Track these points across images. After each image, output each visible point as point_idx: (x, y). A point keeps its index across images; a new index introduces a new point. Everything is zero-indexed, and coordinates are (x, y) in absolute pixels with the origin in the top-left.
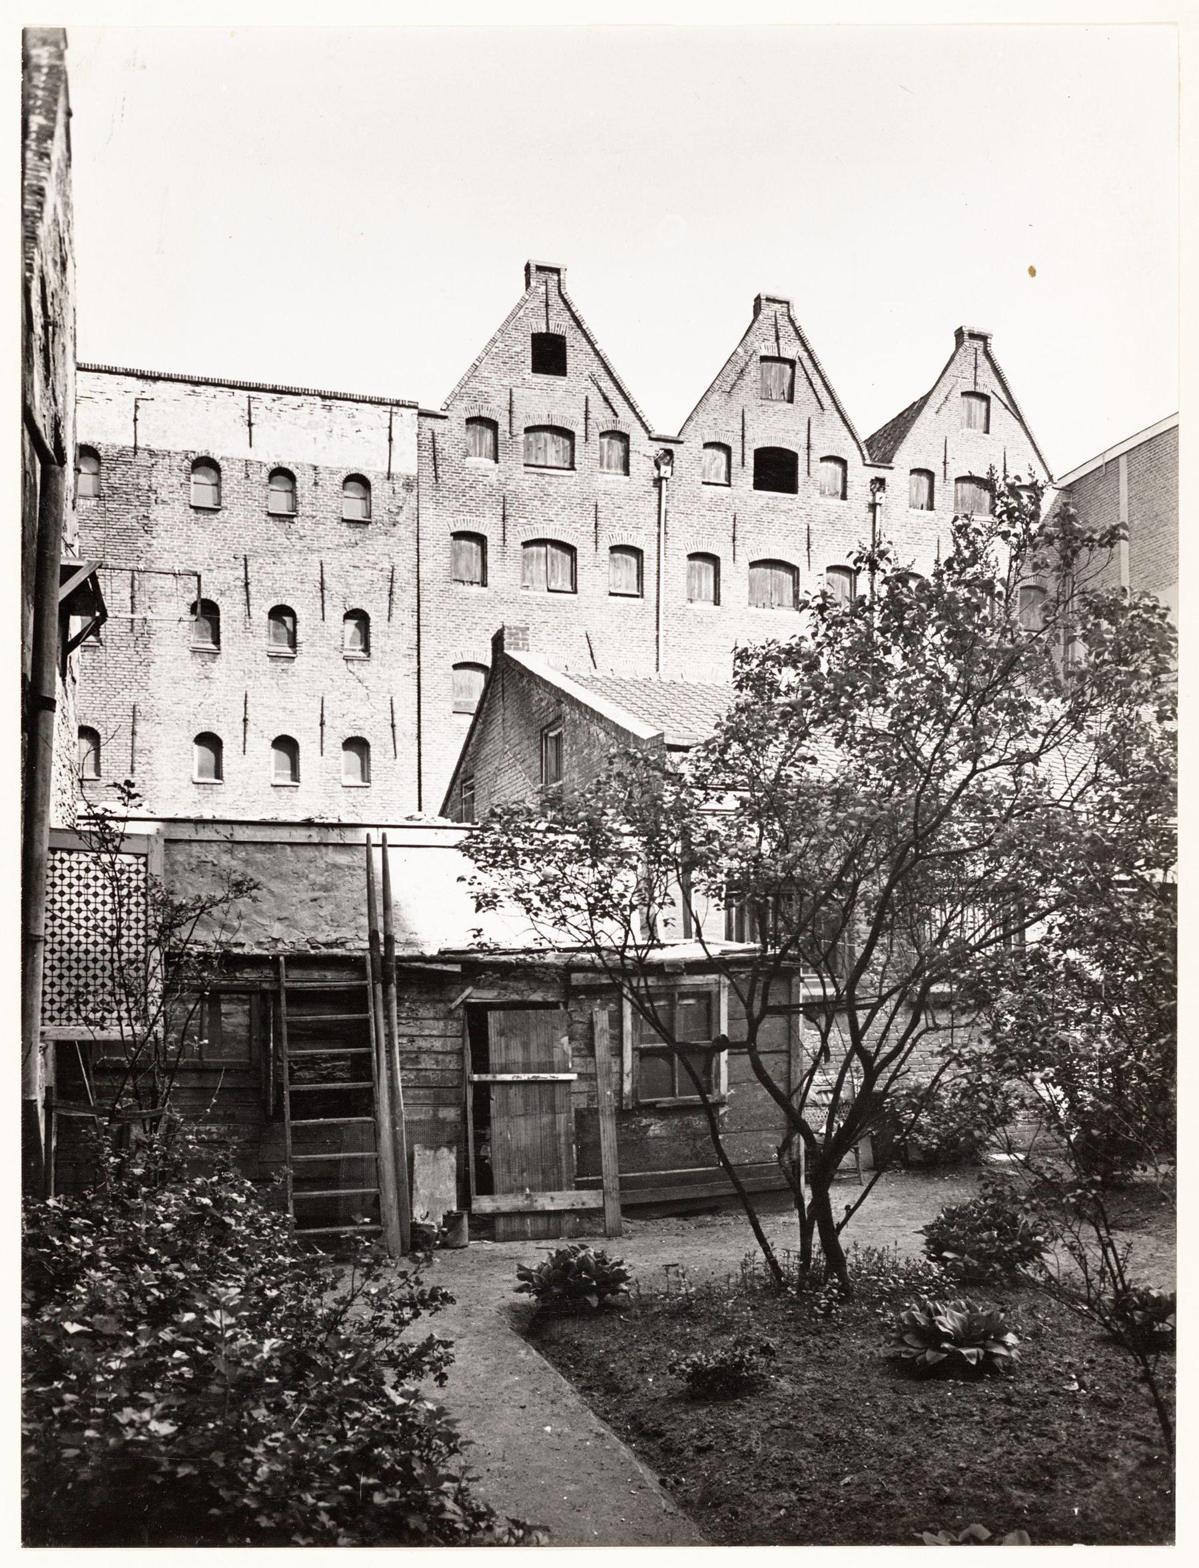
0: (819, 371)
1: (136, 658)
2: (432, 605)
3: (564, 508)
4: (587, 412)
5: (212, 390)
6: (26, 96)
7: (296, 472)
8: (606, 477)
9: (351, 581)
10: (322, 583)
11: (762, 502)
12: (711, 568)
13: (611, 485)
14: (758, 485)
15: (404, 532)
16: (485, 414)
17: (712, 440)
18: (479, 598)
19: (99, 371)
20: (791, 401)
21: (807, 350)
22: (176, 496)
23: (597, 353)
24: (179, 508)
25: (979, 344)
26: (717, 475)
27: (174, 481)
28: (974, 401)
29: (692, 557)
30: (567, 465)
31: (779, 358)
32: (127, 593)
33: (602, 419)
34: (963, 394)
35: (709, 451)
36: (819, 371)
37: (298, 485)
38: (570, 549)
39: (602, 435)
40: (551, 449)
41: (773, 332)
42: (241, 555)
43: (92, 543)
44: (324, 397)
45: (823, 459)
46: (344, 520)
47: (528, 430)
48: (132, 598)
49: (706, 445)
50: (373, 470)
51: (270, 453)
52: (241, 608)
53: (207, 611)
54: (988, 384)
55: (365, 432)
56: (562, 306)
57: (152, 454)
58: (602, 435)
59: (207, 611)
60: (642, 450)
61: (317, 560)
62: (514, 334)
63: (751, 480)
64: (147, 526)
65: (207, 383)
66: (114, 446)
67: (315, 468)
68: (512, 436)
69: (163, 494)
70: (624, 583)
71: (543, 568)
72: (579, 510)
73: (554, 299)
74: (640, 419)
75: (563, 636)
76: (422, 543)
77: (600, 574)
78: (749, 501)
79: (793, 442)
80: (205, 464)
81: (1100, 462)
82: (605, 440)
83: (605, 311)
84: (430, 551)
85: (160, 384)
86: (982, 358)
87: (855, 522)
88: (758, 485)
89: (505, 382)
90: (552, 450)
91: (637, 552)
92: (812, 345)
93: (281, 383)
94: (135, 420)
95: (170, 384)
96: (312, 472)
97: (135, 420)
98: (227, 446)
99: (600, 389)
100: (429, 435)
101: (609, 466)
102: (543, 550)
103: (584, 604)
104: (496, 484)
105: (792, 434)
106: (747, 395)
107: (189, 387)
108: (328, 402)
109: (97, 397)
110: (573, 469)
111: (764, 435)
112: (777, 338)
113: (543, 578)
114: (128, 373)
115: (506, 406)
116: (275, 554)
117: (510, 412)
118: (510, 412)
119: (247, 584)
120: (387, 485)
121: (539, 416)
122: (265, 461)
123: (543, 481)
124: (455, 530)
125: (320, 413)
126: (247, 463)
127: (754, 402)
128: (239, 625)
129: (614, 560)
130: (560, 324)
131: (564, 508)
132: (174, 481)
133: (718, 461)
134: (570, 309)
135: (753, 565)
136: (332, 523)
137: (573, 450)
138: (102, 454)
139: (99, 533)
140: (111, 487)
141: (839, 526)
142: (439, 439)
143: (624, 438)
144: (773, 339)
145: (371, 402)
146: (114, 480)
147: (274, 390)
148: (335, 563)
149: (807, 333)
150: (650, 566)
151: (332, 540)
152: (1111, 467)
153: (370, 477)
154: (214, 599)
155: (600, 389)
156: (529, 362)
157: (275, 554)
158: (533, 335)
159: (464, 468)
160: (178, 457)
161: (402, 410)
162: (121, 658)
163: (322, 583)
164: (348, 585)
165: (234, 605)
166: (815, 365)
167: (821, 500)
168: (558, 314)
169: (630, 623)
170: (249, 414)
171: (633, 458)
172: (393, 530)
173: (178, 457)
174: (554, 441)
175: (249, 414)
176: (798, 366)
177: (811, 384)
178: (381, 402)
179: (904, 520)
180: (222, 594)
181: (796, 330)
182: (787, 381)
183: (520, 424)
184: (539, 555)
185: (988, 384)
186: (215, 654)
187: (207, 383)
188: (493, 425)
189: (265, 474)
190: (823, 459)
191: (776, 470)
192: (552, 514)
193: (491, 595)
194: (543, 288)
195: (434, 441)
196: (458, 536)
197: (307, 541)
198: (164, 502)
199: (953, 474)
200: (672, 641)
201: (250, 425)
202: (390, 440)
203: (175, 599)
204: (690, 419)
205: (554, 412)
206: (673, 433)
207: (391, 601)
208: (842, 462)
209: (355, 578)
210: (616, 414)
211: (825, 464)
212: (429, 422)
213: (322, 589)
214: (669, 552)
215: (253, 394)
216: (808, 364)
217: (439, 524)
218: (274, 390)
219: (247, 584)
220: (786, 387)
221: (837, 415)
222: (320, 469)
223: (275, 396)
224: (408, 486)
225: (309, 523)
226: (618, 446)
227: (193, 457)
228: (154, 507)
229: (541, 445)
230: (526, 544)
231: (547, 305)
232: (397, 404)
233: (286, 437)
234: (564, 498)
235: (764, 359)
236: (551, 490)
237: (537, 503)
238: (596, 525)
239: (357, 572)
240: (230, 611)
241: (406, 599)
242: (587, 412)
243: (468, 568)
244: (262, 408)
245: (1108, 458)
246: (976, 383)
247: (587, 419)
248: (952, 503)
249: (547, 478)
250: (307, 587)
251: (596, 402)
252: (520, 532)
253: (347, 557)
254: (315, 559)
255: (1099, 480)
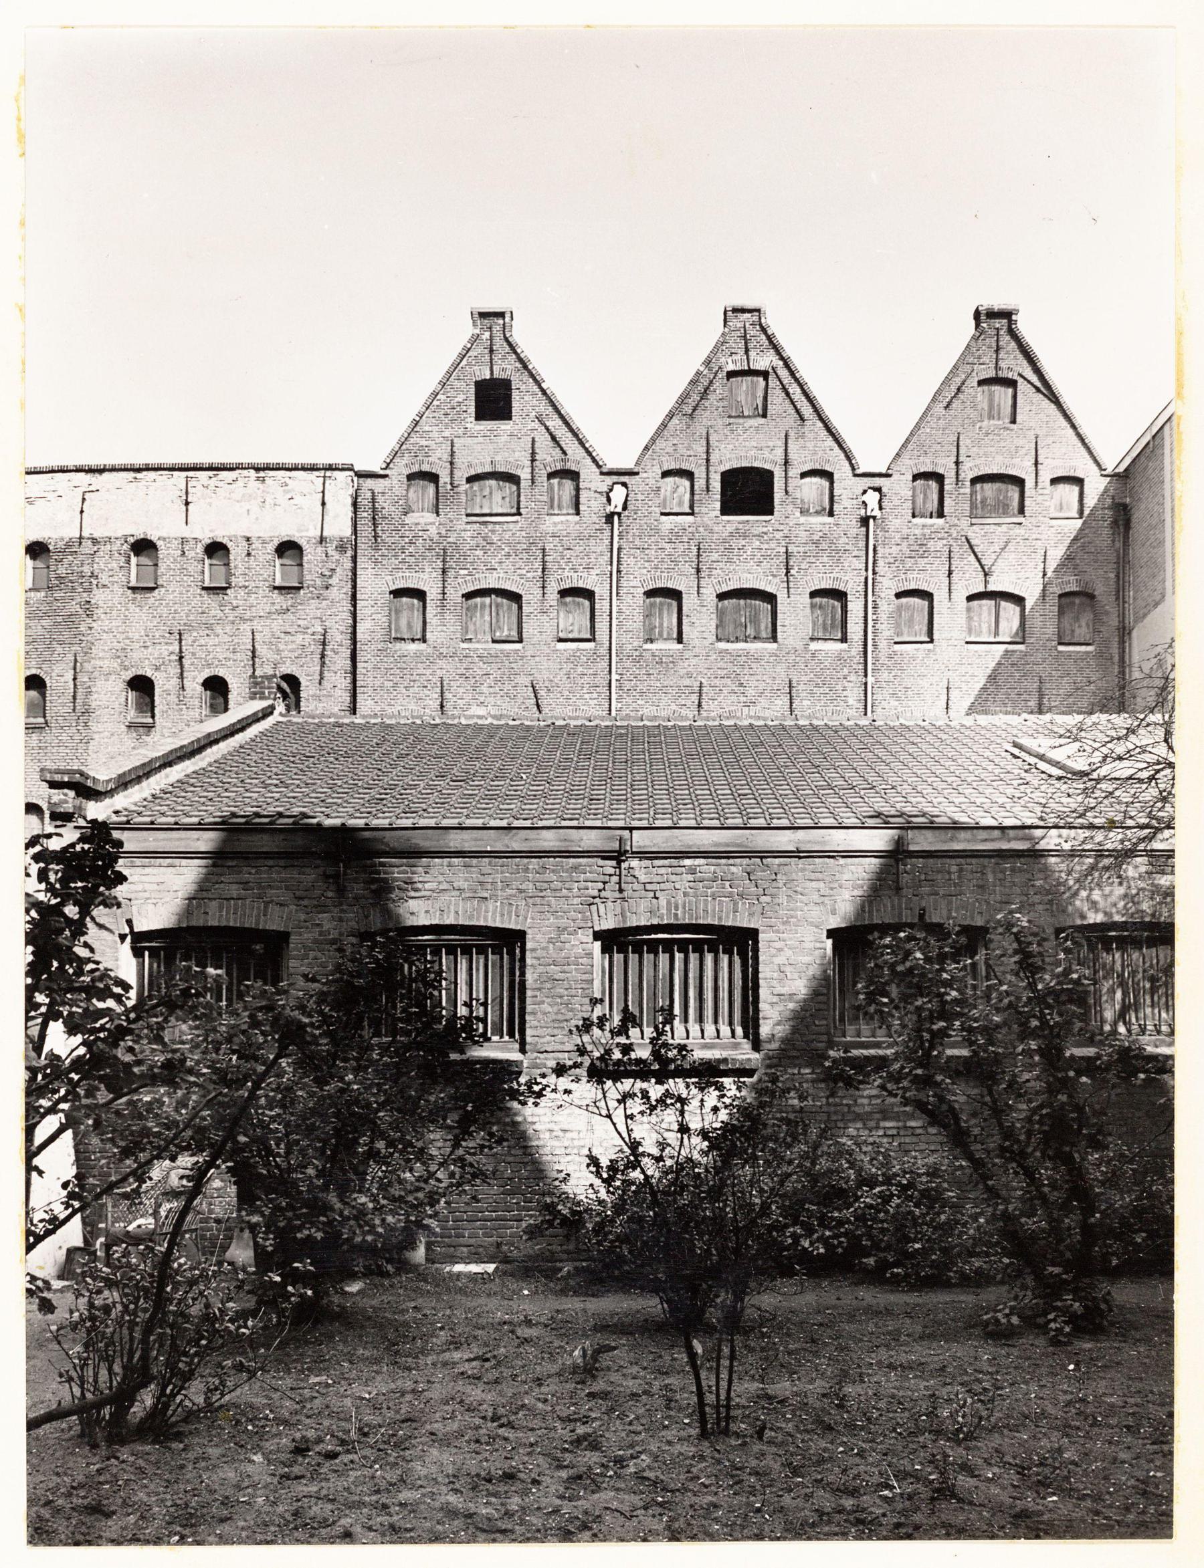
0: (797, 380)
1: (77, 737)
2: (369, 666)
3: (508, 555)
4: (533, 453)
5: (152, 475)
6: (939, 392)
7: (229, 545)
8: (556, 519)
9: (281, 647)
10: (254, 652)
11: (730, 528)
12: (675, 603)
13: (560, 527)
14: (725, 511)
15: (339, 593)
16: (426, 468)
17: (673, 466)
18: (418, 655)
19: (52, 471)
20: (764, 416)
21: (782, 358)
22: (115, 579)
23: (544, 392)
24: (118, 590)
25: (1001, 323)
26: (680, 503)
27: (114, 565)
28: (997, 389)
29: (650, 594)
30: (514, 511)
31: (750, 366)
32: (70, 675)
33: (549, 459)
34: (981, 383)
35: (670, 480)
36: (797, 380)
37: (231, 557)
38: (515, 597)
39: (551, 476)
40: (497, 497)
41: (742, 345)
42: (175, 630)
43: (40, 631)
44: (257, 469)
45: (804, 475)
46: (275, 588)
47: (471, 480)
48: (75, 679)
49: (666, 474)
50: (305, 534)
51: (205, 529)
52: (175, 681)
53: (142, 686)
54: (1014, 365)
55: (298, 500)
56: (507, 349)
57: (95, 541)
58: (551, 476)
59: (142, 686)
60: (593, 486)
61: (249, 629)
62: (457, 384)
63: (718, 505)
64: (88, 609)
65: (148, 468)
66: (62, 539)
67: (248, 539)
68: (453, 486)
69: (104, 578)
70: (576, 628)
71: (487, 618)
72: (525, 556)
73: (499, 343)
74: (589, 453)
75: (507, 687)
76: (360, 604)
77: (546, 620)
78: (716, 529)
79: (765, 457)
80: (143, 547)
81: (1148, 437)
82: (555, 481)
83: (546, 346)
84: (368, 611)
85: (106, 475)
86: (1005, 339)
87: (844, 539)
88: (725, 511)
89: (446, 434)
90: (497, 497)
91: (589, 594)
92: (788, 352)
93: (217, 460)
94: (82, 512)
95: (115, 474)
96: (245, 543)
97: (82, 512)
98: (163, 524)
99: (547, 429)
100: (369, 495)
101: (560, 508)
102: (487, 600)
103: (529, 653)
104: (436, 537)
105: (766, 452)
106: (710, 417)
107: (132, 474)
108: (262, 474)
109: (50, 496)
110: (519, 514)
111: (729, 456)
112: (747, 351)
113: (487, 629)
114: (78, 470)
115: (446, 457)
116: (210, 627)
117: (452, 463)
118: (452, 463)
119: (181, 658)
120: (320, 549)
121: (482, 464)
122: (200, 537)
123: (485, 530)
124: (394, 588)
125: (254, 484)
126: (184, 541)
127: (720, 422)
128: (173, 698)
129: (566, 604)
130: (505, 368)
131: (508, 555)
132: (114, 565)
133: (681, 489)
134: (515, 352)
135: (722, 596)
136: (264, 590)
137: (519, 496)
138: (51, 547)
139: (46, 622)
140: (59, 578)
141: (824, 546)
142: (380, 498)
143: (574, 476)
144: (742, 352)
145: (303, 469)
146: (62, 570)
147: (211, 468)
148: (267, 631)
149: (782, 339)
150: (601, 606)
151: (263, 607)
152: (1158, 440)
153: (302, 542)
154: (149, 674)
155: (547, 429)
156: (472, 410)
157: (210, 627)
158: (477, 383)
159: (403, 525)
160: (118, 542)
161: (336, 473)
162: (64, 737)
163: (254, 652)
164: (278, 651)
165: (168, 679)
166: (792, 374)
167: (803, 520)
168: (504, 358)
169: (580, 669)
170: (187, 493)
171: (584, 496)
172: (326, 593)
173: (118, 542)
174: (500, 488)
175: (187, 493)
176: (772, 377)
177: (788, 394)
178: (313, 468)
179: (905, 531)
180: (157, 669)
181: (769, 338)
182: (760, 394)
183: (461, 475)
184: (483, 606)
185: (1014, 365)
186: (149, 727)
187: (148, 468)
188: (433, 478)
189: (200, 549)
190: (804, 475)
191: (748, 492)
192: (494, 563)
193: (430, 650)
194: (487, 335)
195: (373, 500)
196: (398, 593)
197: (240, 611)
198: (104, 586)
199: (968, 474)
200: (627, 685)
201: (187, 504)
202: (323, 504)
203: (113, 677)
204: (646, 448)
205: (498, 458)
206: (629, 464)
207: (323, 664)
208: (828, 476)
209: (286, 643)
210: (564, 453)
211: (807, 480)
212: (369, 483)
213: (254, 657)
214: (623, 591)
215: (191, 474)
216: (783, 373)
217: (375, 584)
218: (211, 468)
219: (181, 658)
220: (760, 402)
221: (820, 424)
222: (253, 540)
223: (211, 473)
224: (341, 548)
225: (242, 592)
226: (568, 485)
227: (132, 540)
228: (95, 591)
229: (486, 492)
230: (468, 596)
231: (491, 351)
232: (330, 468)
233: (226, 512)
234: (509, 544)
235: (731, 375)
236: (495, 538)
237: (479, 553)
238: (544, 570)
239: (288, 638)
240: (164, 684)
241: (341, 661)
242: (533, 453)
243: (410, 626)
244: (199, 487)
245: (1155, 430)
246: (997, 368)
247: (533, 460)
248: (967, 507)
249: (490, 527)
250: (238, 656)
251: (543, 440)
252: (462, 583)
253: (278, 624)
254: (246, 628)
255: (1149, 458)
